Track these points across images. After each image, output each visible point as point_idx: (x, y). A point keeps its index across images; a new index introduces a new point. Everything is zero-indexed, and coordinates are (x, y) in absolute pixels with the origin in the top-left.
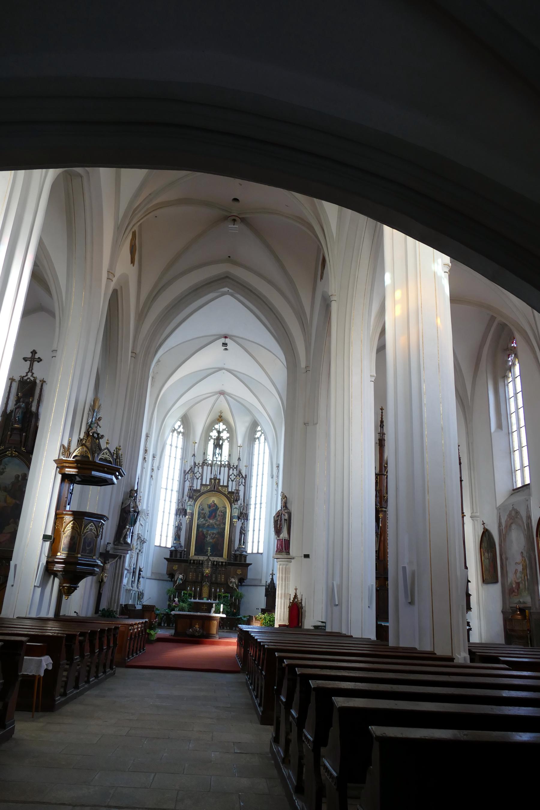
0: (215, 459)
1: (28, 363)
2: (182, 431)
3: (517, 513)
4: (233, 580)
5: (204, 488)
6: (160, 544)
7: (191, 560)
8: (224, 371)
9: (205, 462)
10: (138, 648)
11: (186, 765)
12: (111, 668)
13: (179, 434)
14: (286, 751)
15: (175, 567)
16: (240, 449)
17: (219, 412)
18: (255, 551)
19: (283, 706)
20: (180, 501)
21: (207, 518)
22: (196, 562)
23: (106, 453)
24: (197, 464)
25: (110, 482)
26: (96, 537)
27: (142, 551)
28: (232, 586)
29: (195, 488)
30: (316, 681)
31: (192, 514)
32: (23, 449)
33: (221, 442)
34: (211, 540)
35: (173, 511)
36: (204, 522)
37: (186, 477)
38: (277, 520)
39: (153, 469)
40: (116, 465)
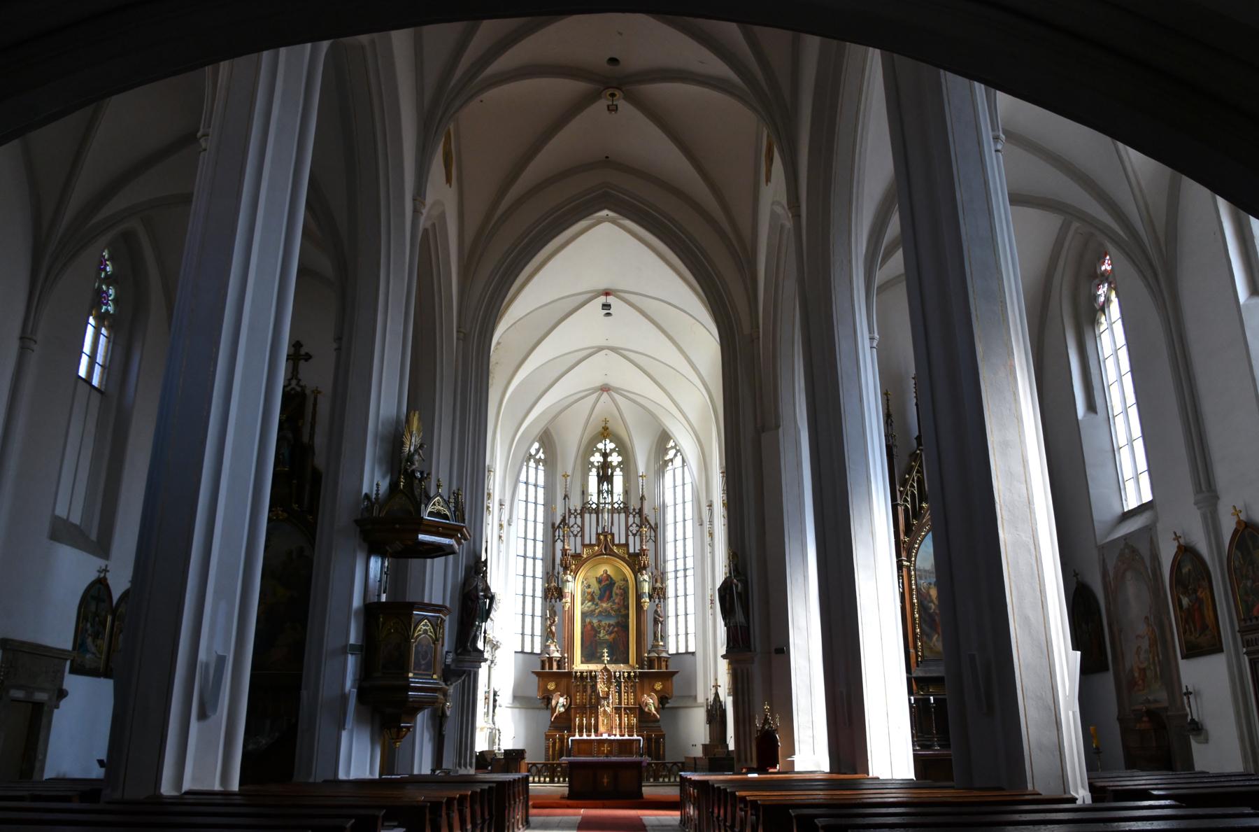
0: (602, 501)
2: (543, 457)
3: (1134, 551)
13: (539, 462)
15: (551, 686)
18: (682, 650)
21: (597, 600)
22: (585, 674)
24: (573, 511)
25: (448, 551)
26: (434, 643)
32: (295, 506)
33: (610, 471)
34: (607, 637)
37: (557, 534)
38: (725, 596)
39: (501, 526)
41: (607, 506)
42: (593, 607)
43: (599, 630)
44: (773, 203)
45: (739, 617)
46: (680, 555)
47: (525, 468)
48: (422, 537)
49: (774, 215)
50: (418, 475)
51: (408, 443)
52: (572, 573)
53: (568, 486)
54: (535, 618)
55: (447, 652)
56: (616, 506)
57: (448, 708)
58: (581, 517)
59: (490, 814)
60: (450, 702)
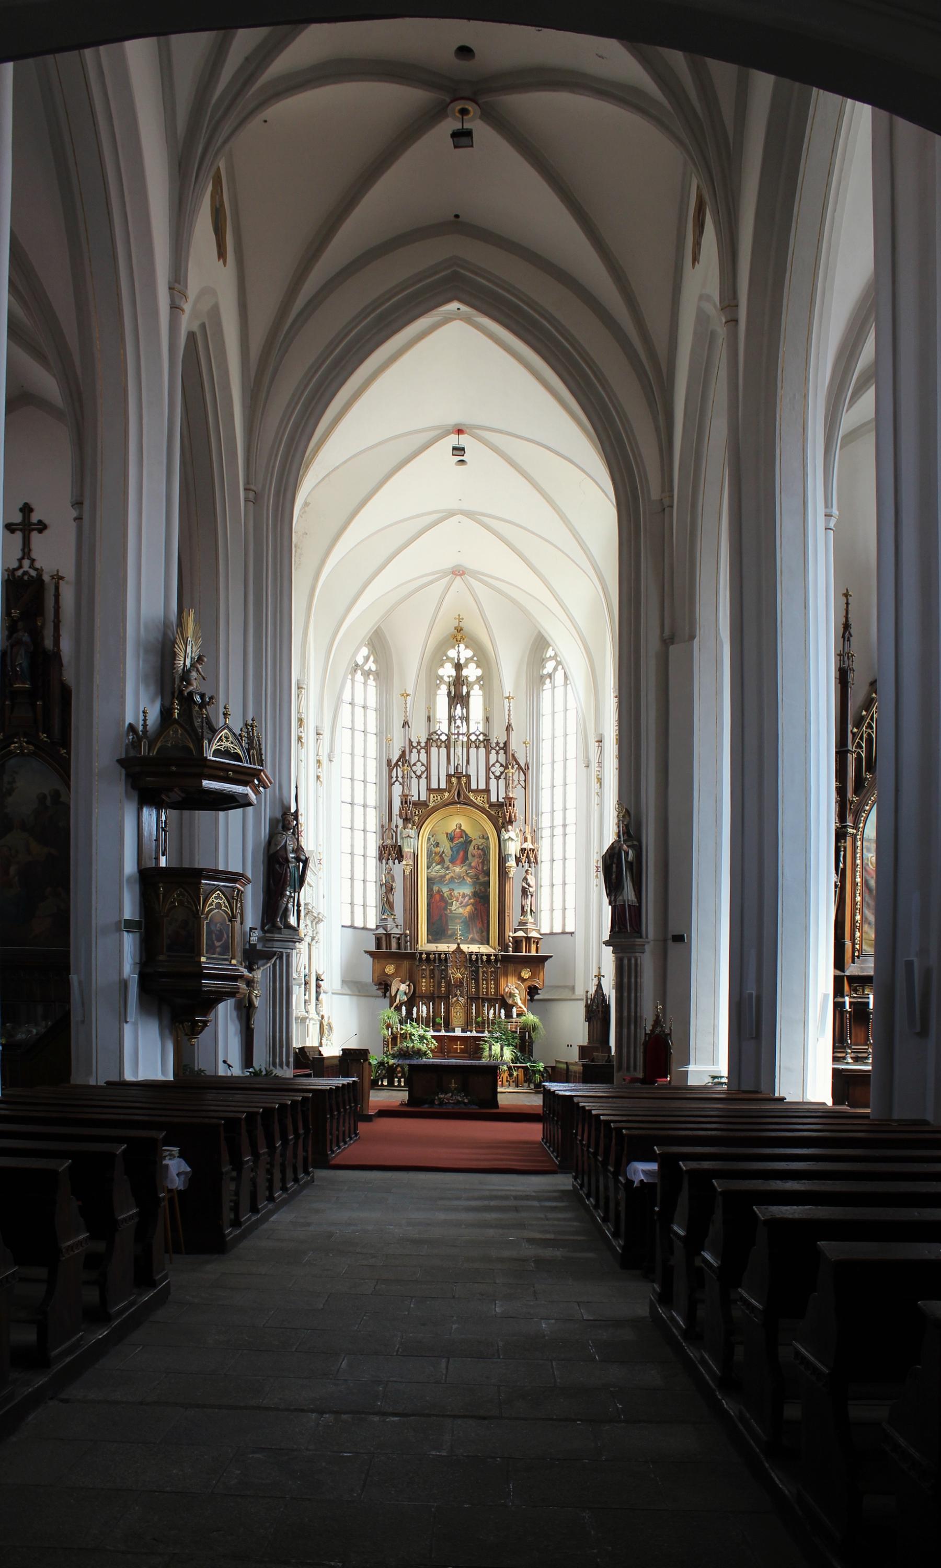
1: (18, 535)
2: (374, 668)
5: (436, 798)
7: (423, 953)
8: (459, 517)
9: (432, 739)
10: (347, 1132)
12: (307, 1172)
13: (368, 675)
14: (690, 1317)
15: (390, 969)
16: (509, 703)
17: (455, 618)
18: (558, 929)
20: (385, 829)
21: (447, 863)
22: (432, 956)
23: (225, 737)
24: (415, 744)
25: (242, 801)
26: (230, 921)
27: (318, 939)
29: (415, 798)
31: (416, 857)
32: (43, 736)
33: (465, 690)
34: (461, 910)
35: (373, 851)
36: (443, 872)
37: (394, 774)
38: (611, 865)
40: (251, 764)
41: (461, 737)
42: (443, 872)
44: (701, 298)
45: (629, 893)
46: (558, 806)
47: (349, 683)
48: (206, 783)
49: (702, 318)
50: (198, 699)
51: (183, 655)
53: (408, 709)
54: (368, 883)
55: (251, 929)
56: (473, 738)
58: (426, 752)
59: (306, 1127)
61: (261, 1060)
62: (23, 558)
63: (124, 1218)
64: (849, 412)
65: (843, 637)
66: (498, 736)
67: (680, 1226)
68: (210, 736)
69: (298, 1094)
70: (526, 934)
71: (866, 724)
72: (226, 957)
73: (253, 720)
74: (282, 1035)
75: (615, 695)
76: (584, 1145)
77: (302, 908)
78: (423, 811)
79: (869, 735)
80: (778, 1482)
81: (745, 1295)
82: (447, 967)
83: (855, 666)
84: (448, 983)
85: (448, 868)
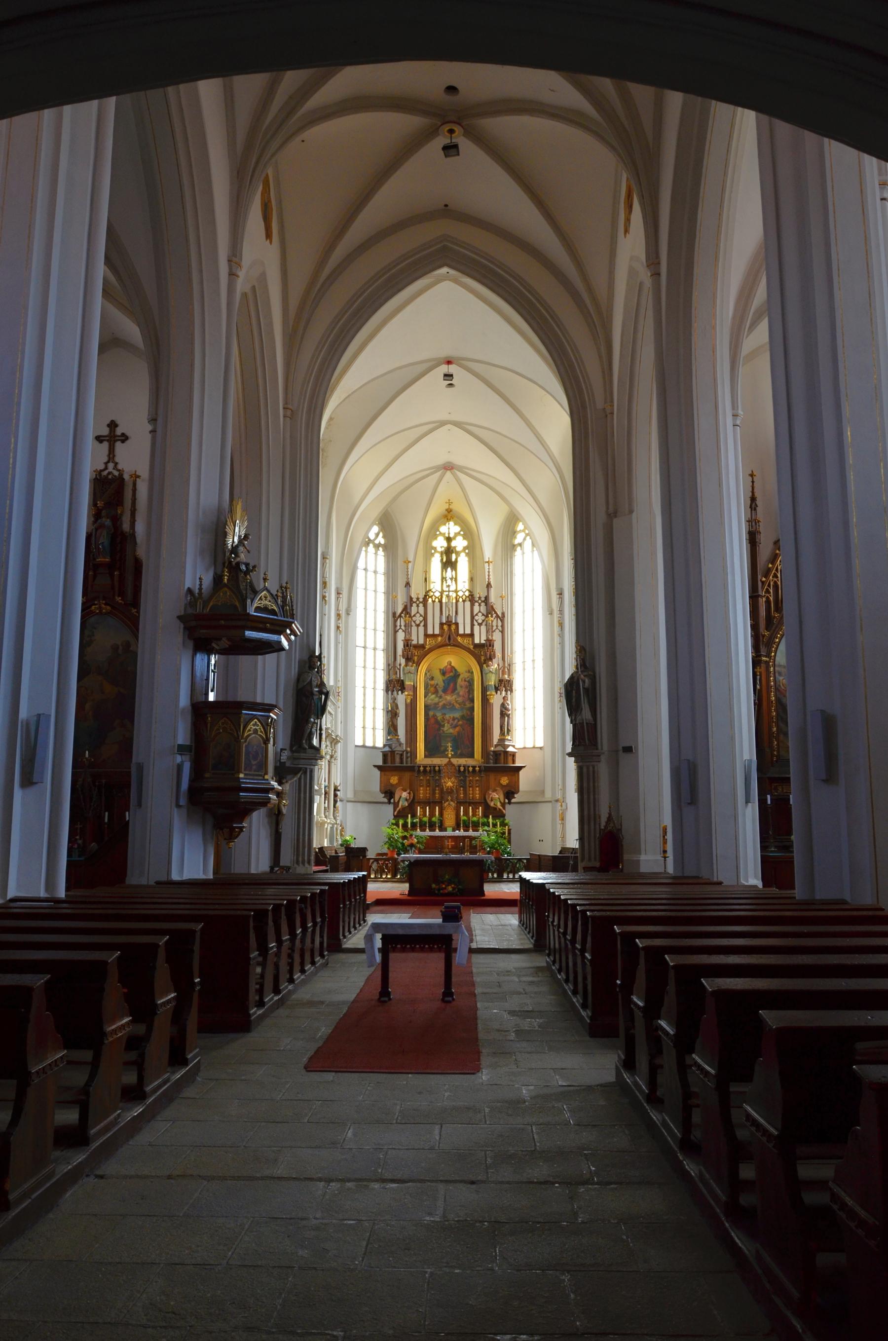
0: (445, 589)
1: (106, 445)
2: (383, 542)
4: (495, 795)
6: (364, 741)
11: (486, 1109)
12: (322, 956)
13: (378, 547)
14: (652, 1084)
15: (394, 780)
16: (489, 566)
17: (446, 503)
19: (640, 1013)
20: (391, 667)
21: (440, 693)
22: (428, 769)
24: (414, 600)
25: (276, 647)
28: (494, 806)
29: (415, 642)
30: (712, 979)
31: (415, 689)
32: (118, 599)
33: (454, 557)
34: (451, 731)
36: (437, 700)
37: (398, 623)
40: (284, 617)
42: (437, 700)
43: (442, 723)
45: (586, 714)
48: (249, 634)
49: (632, 273)
50: (243, 567)
51: (232, 534)
52: (415, 665)
53: (409, 573)
54: (376, 711)
55: (282, 750)
57: (284, 806)
59: (322, 916)
60: (286, 800)
61: (286, 858)
62: (108, 462)
63: (163, 1003)
64: (748, 338)
65: (751, 507)
66: (480, 592)
67: (639, 998)
68: (252, 596)
69: (317, 887)
70: (504, 749)
71: (772, 574)
72: (260, 773)
73: (287, 583)
74: (305, 838)
75: (572, 558)
76: (555, 926)
77: (324, 732)
78: (421, 652)
79: (775, 583)
80: (738, 1241)
81: (699, 1061)
82: (440, 777)
83: (761, 530)
84: (442, 790)
85: (441, 697)
